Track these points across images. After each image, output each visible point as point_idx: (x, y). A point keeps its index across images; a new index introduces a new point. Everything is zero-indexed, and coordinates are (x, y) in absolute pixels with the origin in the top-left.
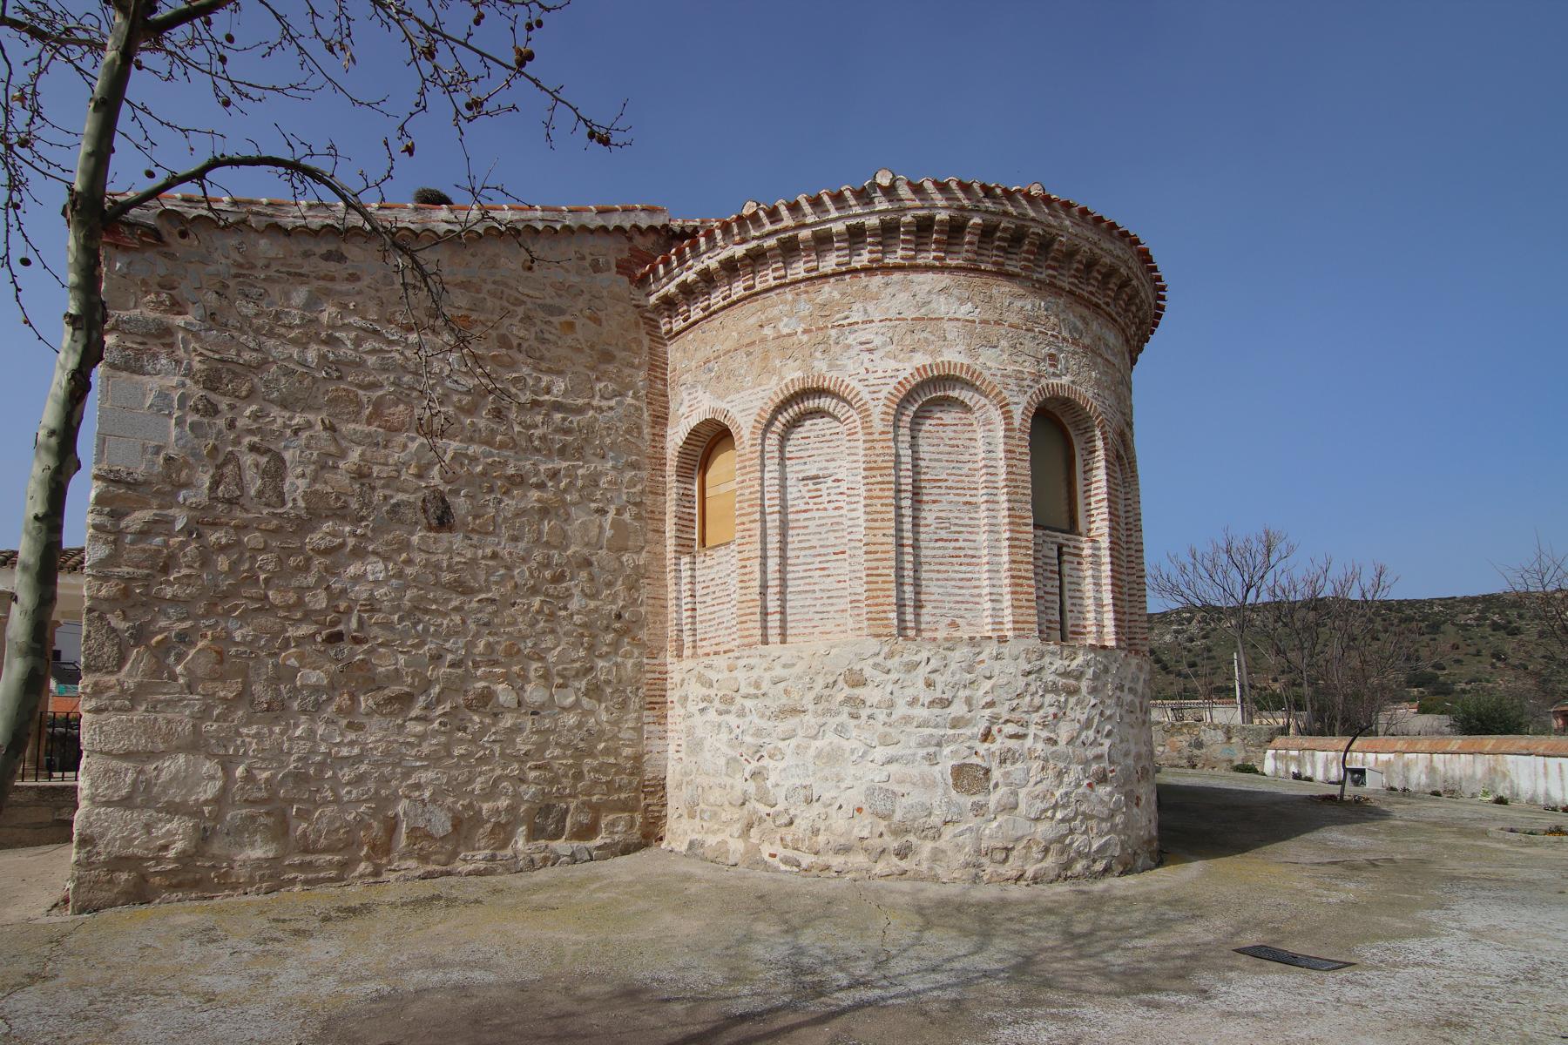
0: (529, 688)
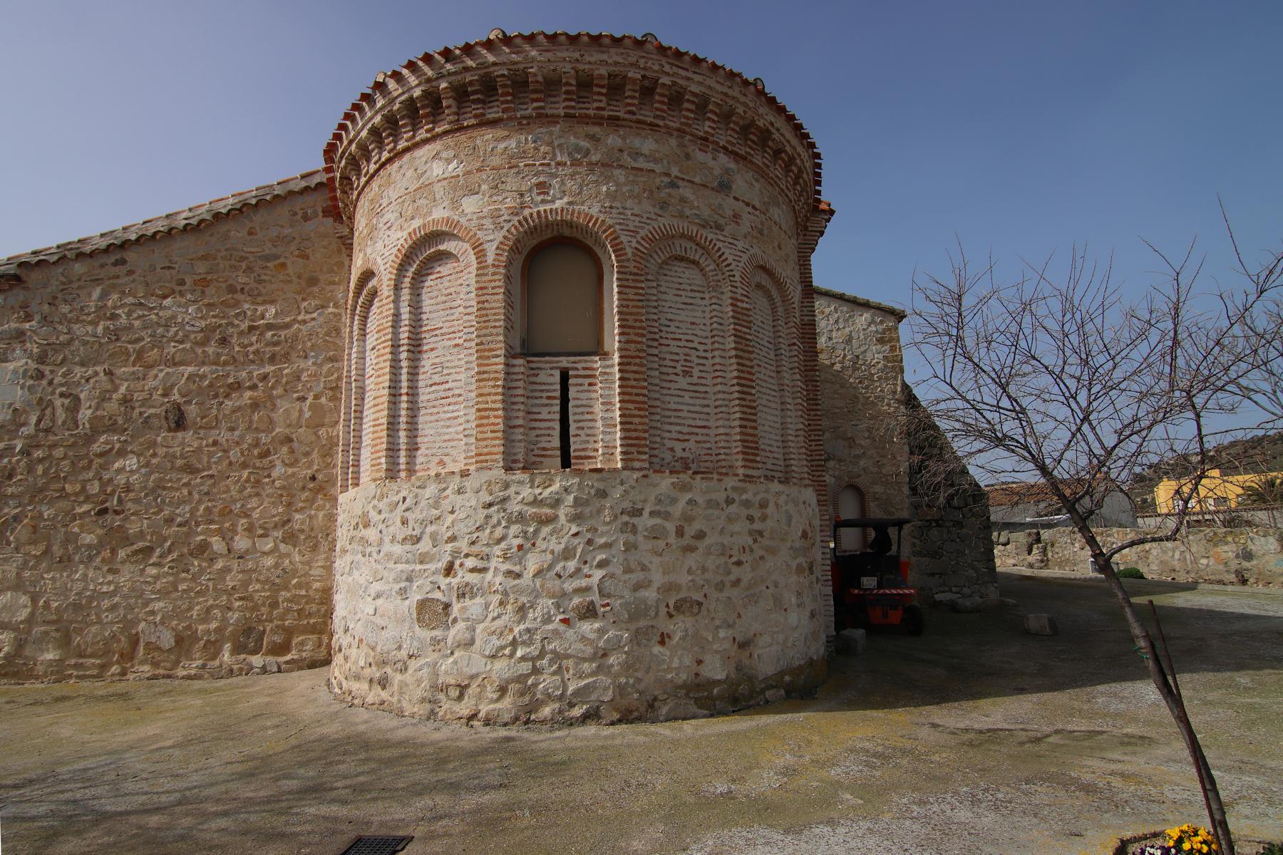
0: (237, 538)
